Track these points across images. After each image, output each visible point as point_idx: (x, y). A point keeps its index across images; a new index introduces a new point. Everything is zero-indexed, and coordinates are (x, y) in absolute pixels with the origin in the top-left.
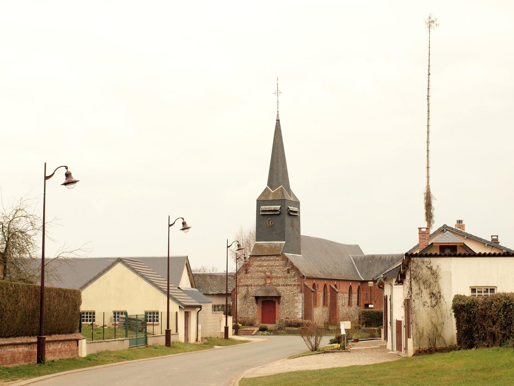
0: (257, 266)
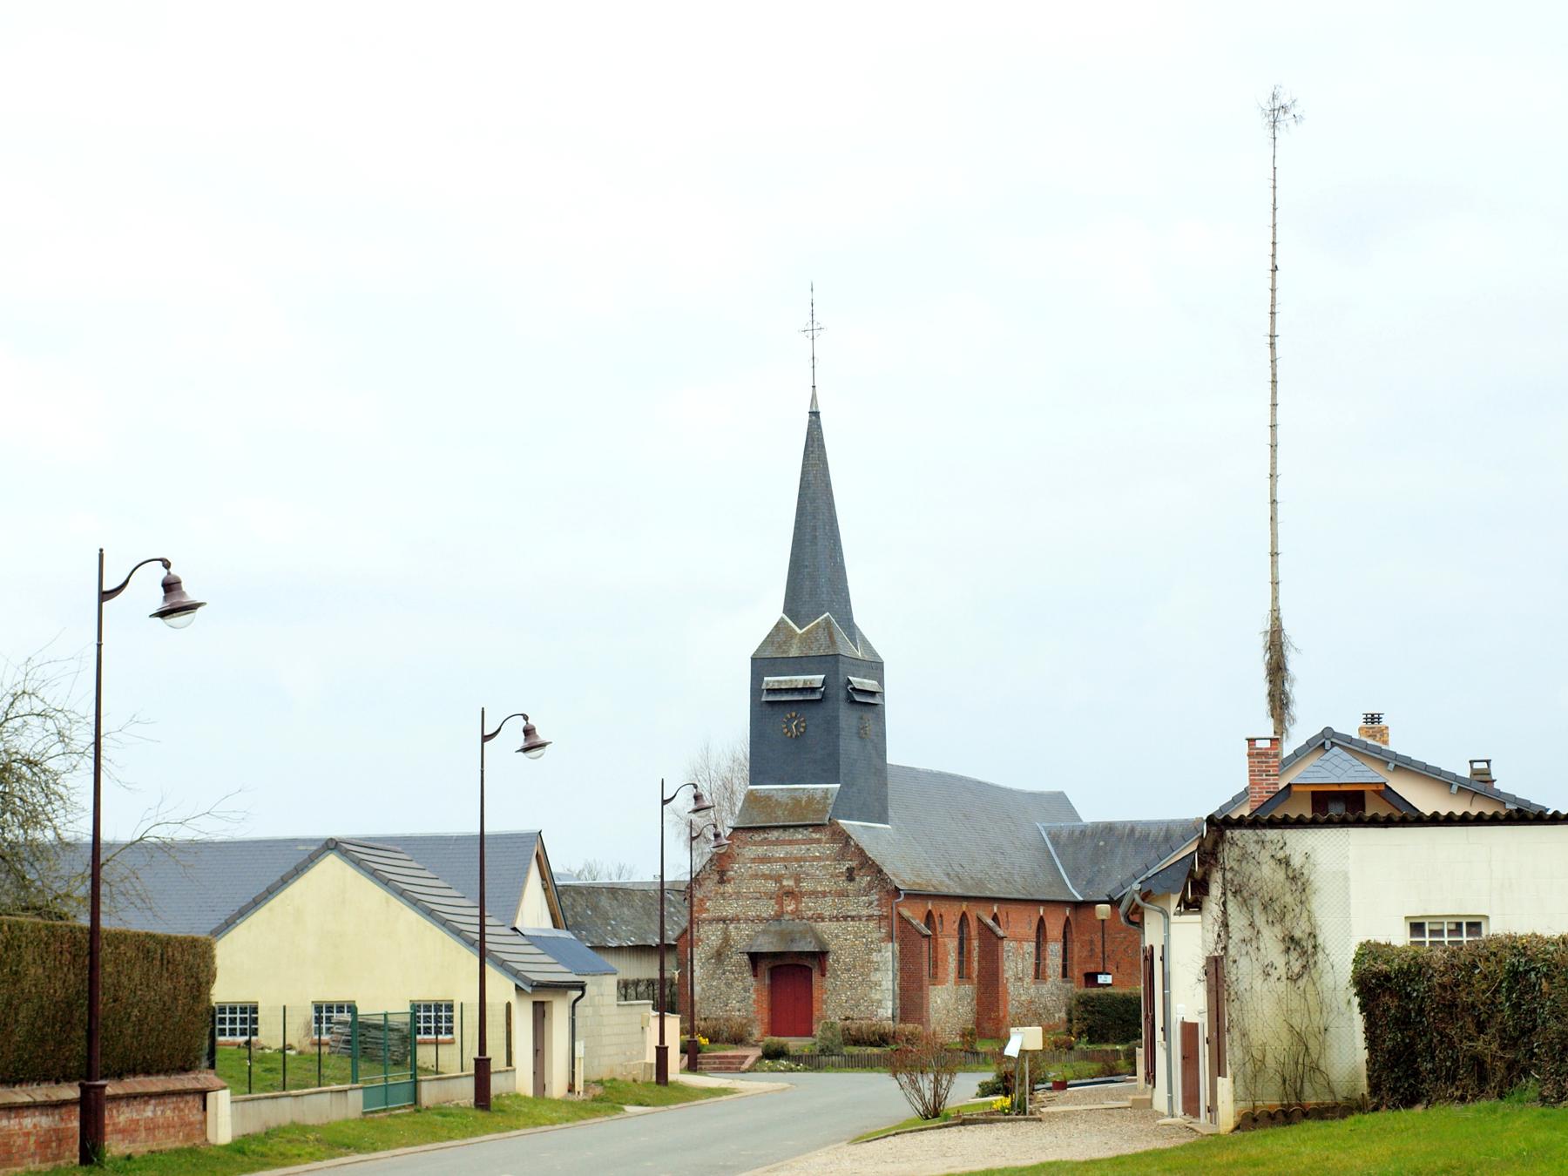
0: (753, 860)
